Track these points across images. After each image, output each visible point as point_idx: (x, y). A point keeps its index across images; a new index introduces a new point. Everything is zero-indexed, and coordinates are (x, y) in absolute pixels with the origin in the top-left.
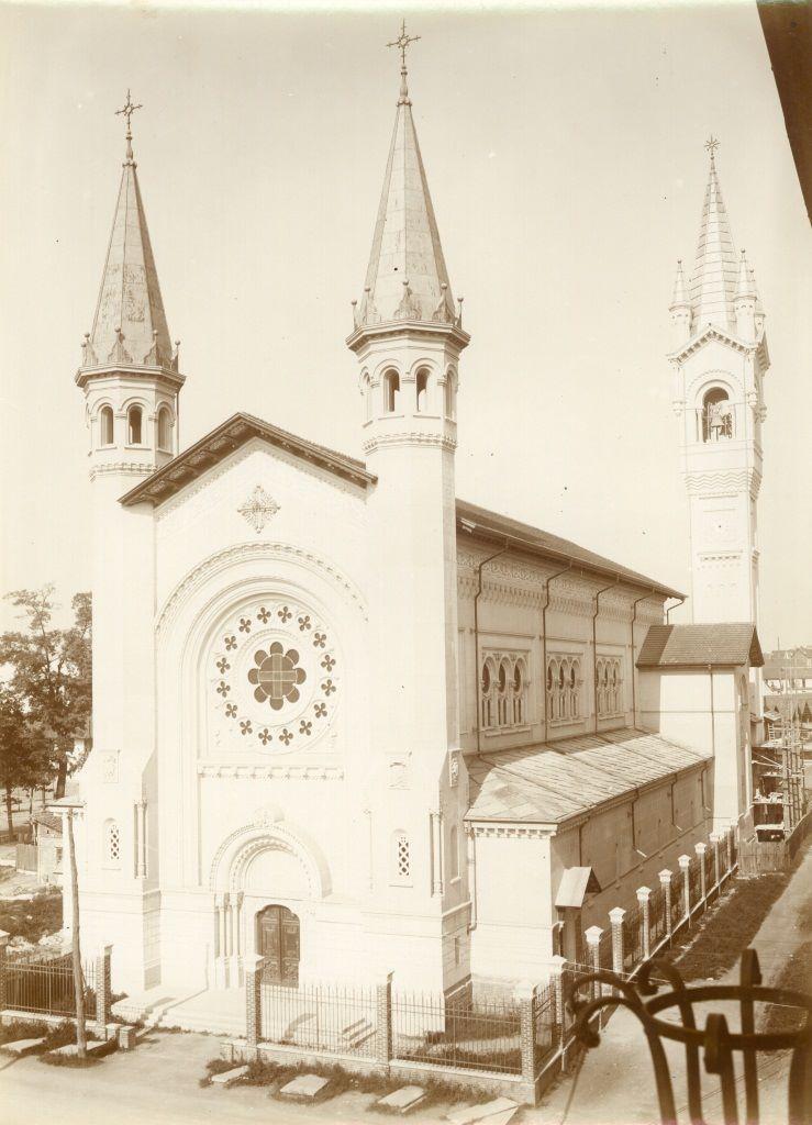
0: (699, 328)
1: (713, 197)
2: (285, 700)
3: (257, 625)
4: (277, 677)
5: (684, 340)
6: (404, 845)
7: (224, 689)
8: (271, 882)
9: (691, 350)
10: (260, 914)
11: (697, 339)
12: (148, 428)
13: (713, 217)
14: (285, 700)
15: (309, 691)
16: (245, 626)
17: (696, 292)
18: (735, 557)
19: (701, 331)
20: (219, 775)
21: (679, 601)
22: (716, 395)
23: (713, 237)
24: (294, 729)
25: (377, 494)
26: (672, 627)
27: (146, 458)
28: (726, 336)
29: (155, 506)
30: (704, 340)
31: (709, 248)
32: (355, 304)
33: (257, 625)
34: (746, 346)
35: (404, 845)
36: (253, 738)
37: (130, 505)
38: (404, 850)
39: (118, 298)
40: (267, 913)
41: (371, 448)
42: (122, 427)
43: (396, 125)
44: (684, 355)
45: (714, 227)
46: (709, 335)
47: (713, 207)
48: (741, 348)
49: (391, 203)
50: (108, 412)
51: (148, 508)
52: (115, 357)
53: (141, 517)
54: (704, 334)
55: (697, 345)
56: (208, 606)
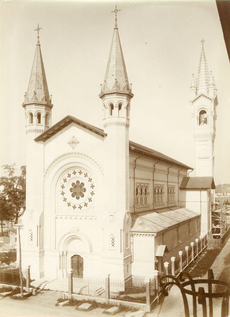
0: (198, 93)
1: (203, 56)
2: (80, 197)
3: (72, 175)
4: (78, 190)
5: (194, 97)
6: (113, 238)
7: (63, 194)
8: (75, 248)
9: (196, 99)
10: (72, 257)
11: (198, 96)
12: (43, 119)
13: (203, 62)
14: (80, 197)
15: (87, 194)
16: (69, 176)
17: (197, 83)
18: (208, 158)
19: (199, 94)
20: (61, 218)
21: (192, 170)
22: (203, 112)
23: (203, 68)
24: (83, 205)
25: (107, 139)
26: (190, 177)
27: (42, 128)
28: (206, 95)
29: (44, 141)
30: (199, 96)
31: (201, 70)
32: (101, 85)
33: (72, 175)
34: (212, 98)
35: (113, 238)
36: (71, 207)
37: (37, 141)
38: (113, 240)
39: (34, 82)
40: (74, 257)
41: (105, 126)
42: (35, 119)
43: (114, 34)
44: (194, 101)
45: (203, 65)
46: (201, 95)
47: (203, 59)
48: (210, 99)
49: (112, 57)
50: (31, 115)
51: (42, 142)
52: (34, 99)
53: (40, 145)
54: (200, 95)
55: (198, 98)
56: (55, 174)
